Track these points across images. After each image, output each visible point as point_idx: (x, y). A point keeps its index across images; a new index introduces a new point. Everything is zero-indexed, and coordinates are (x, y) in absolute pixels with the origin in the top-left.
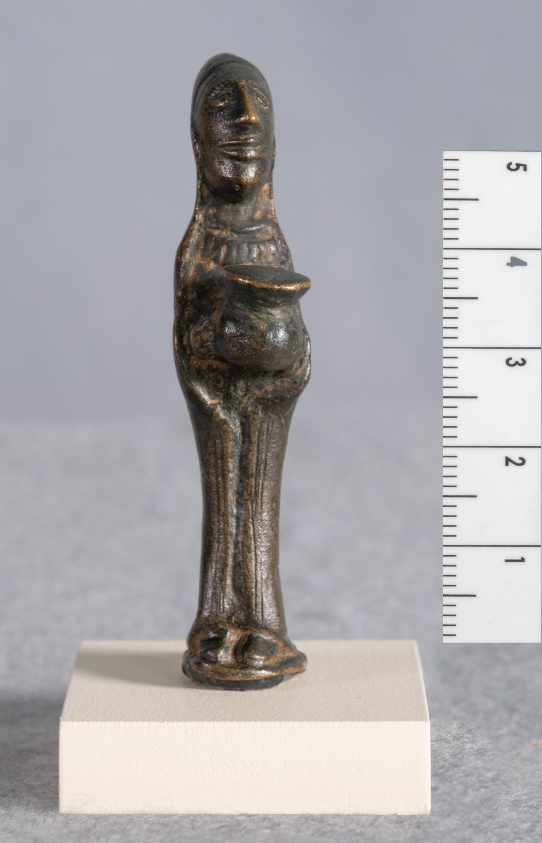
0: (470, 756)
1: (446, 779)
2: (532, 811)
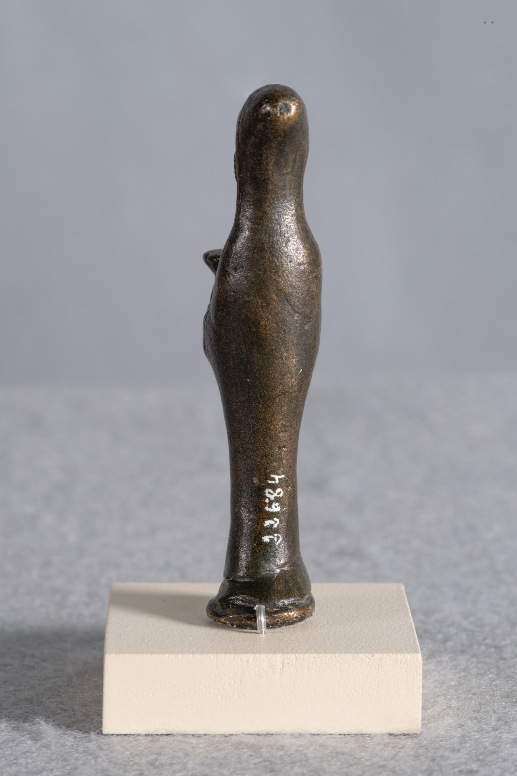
0: (506, 744)
1: (486, 764)
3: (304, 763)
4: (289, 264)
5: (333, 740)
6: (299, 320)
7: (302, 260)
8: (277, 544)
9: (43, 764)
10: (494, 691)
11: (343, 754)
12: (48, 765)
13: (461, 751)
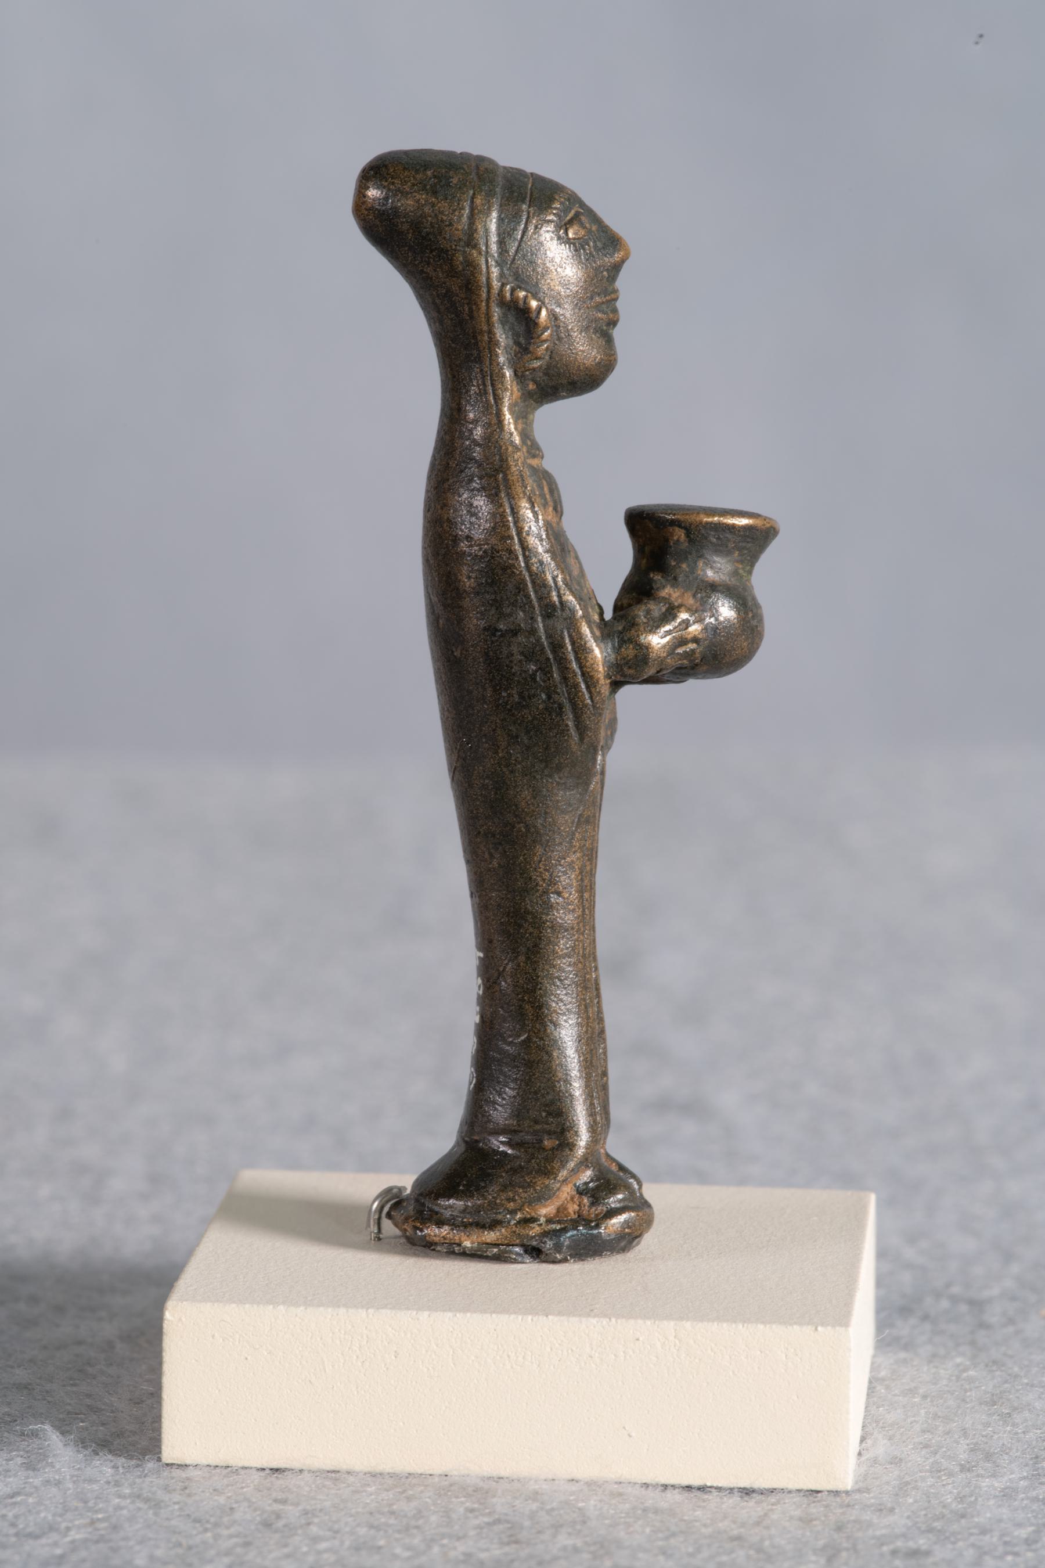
2: (1035, 1507)
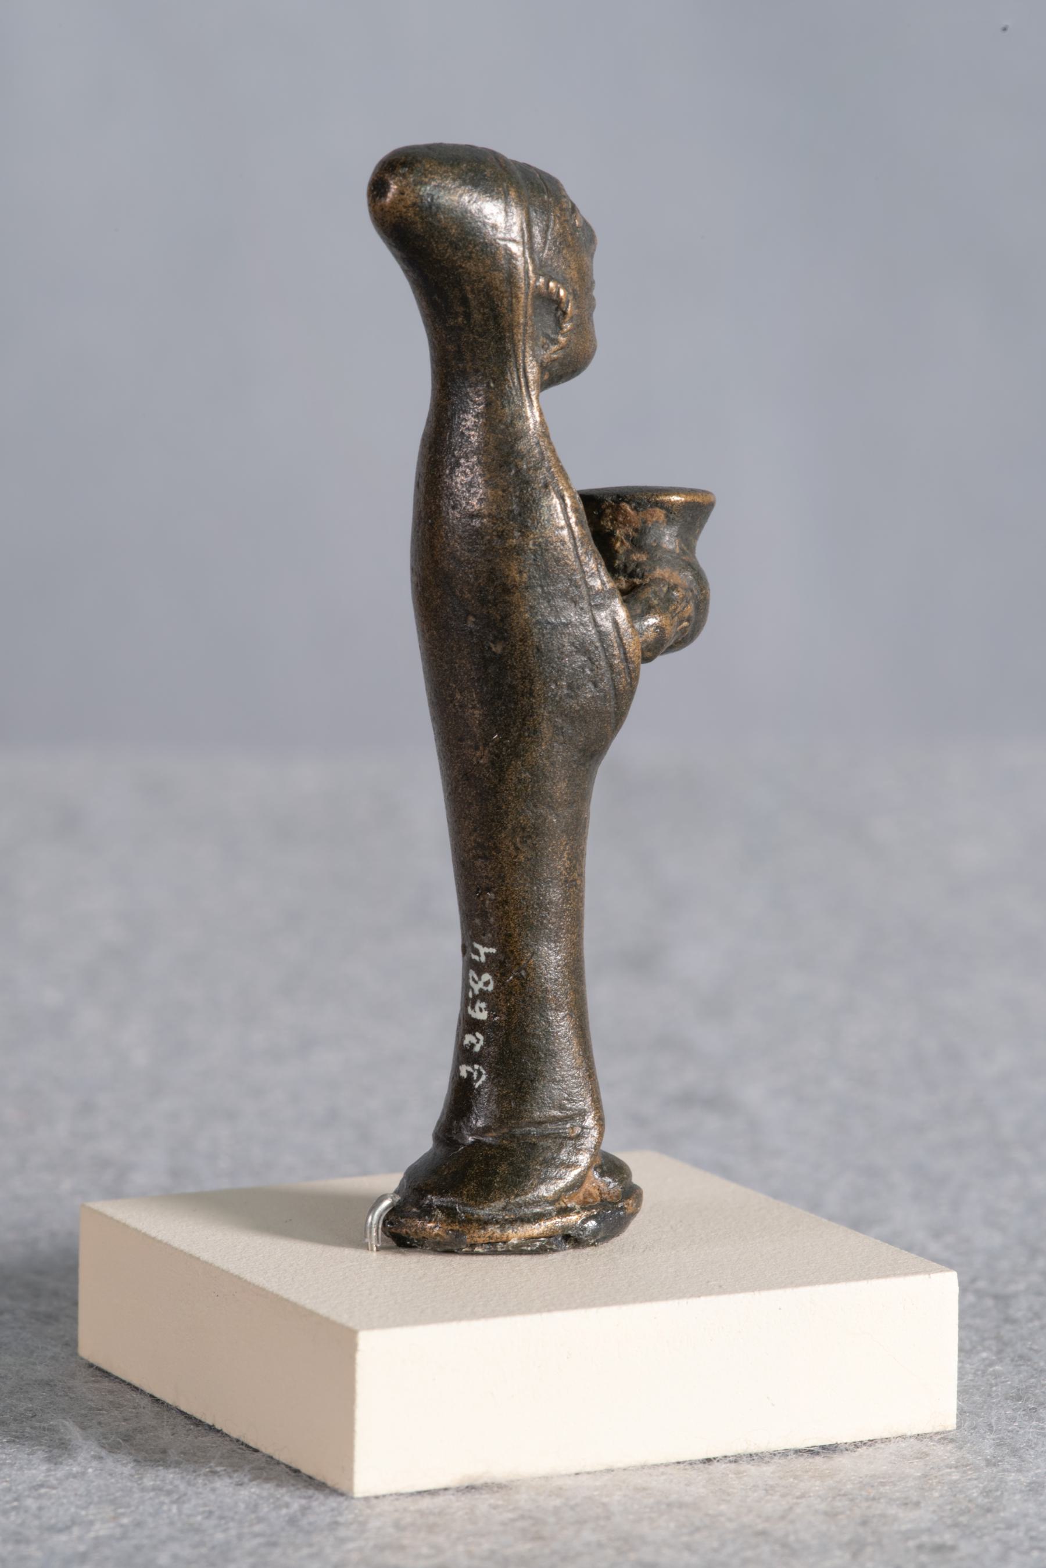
0: (1014, 1494)
3: (602, 1523)
4: (451, 511)
5: (663, 1478)
6: (478, 631)
7: (477, 507)
8: (477, 1085)
9: (73, 1510)
10: (992, 1386)
11: (681, 1505)
12: (83, 1513)
13: (922, 1505)
